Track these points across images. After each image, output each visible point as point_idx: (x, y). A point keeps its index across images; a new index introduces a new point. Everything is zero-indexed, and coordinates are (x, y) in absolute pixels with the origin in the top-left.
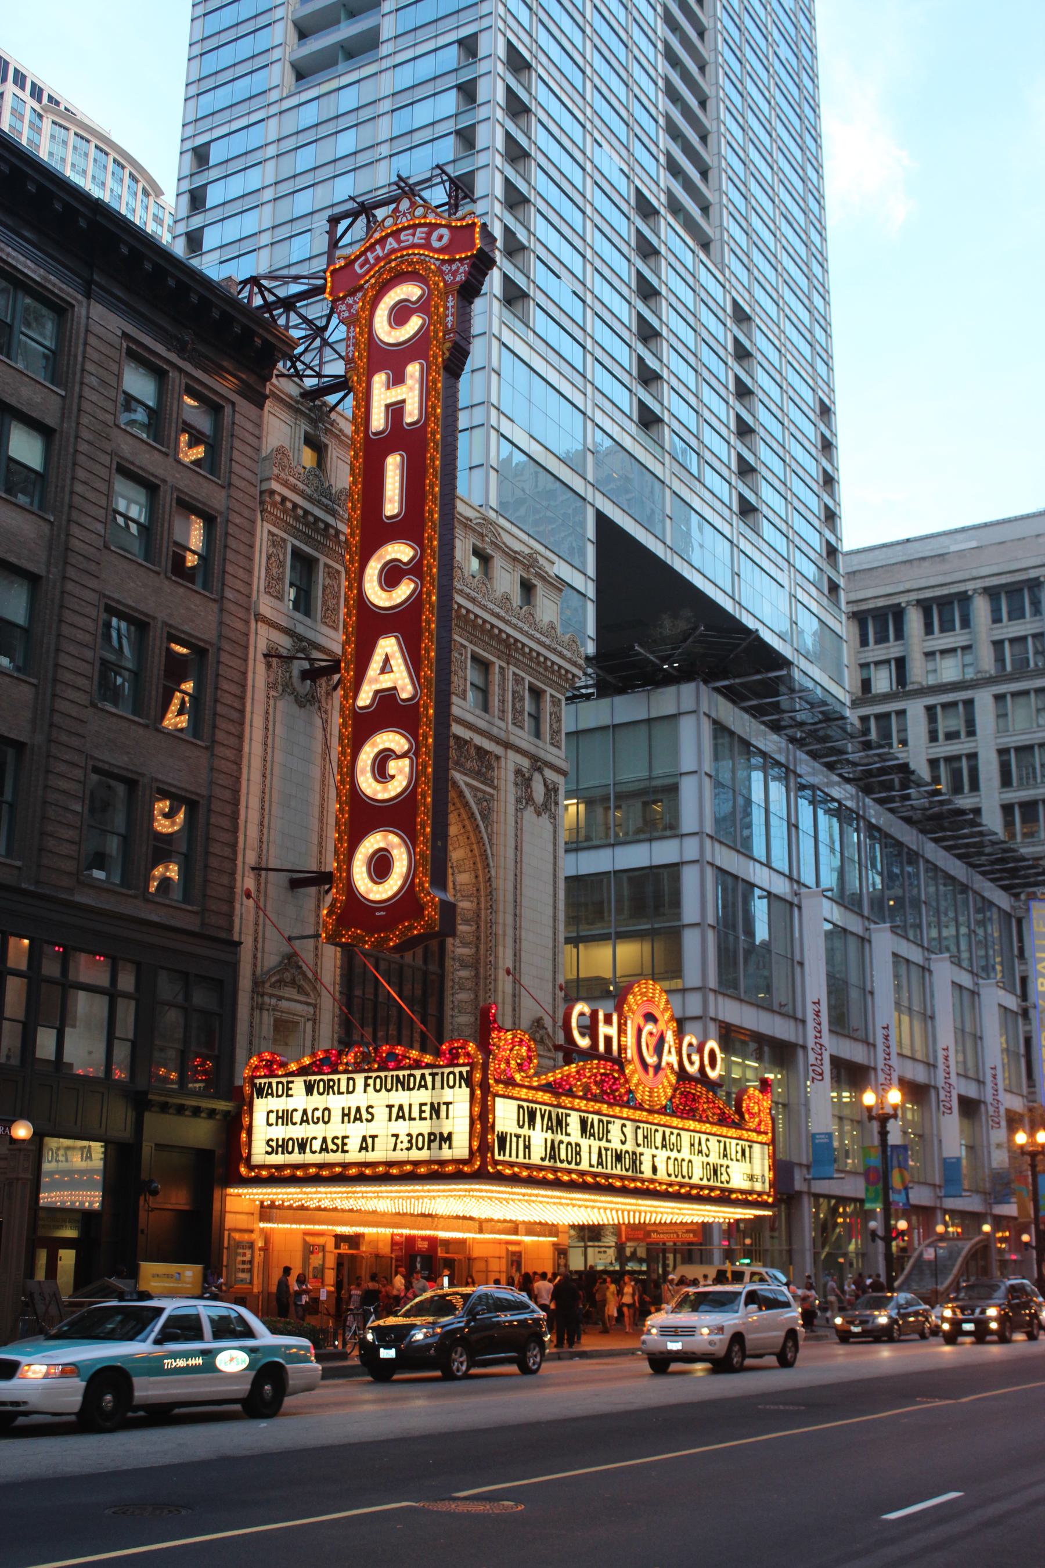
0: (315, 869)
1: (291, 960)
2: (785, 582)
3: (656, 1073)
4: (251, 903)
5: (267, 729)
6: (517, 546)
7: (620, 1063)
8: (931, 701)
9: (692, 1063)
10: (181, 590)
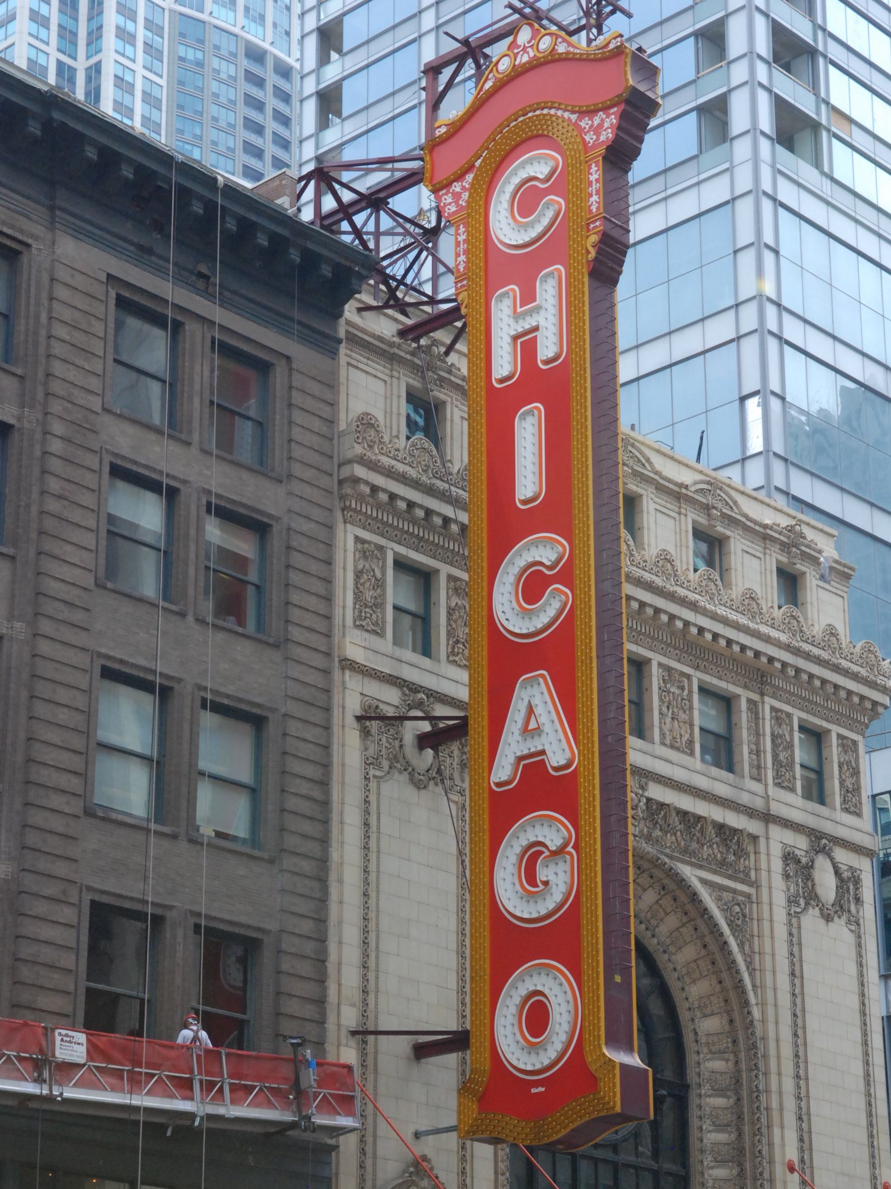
0: (455, 1029)
5: (366, 824)
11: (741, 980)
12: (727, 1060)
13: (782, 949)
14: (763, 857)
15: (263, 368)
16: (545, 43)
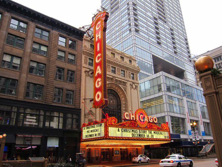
7: (135, 121)
15: (75, 42)
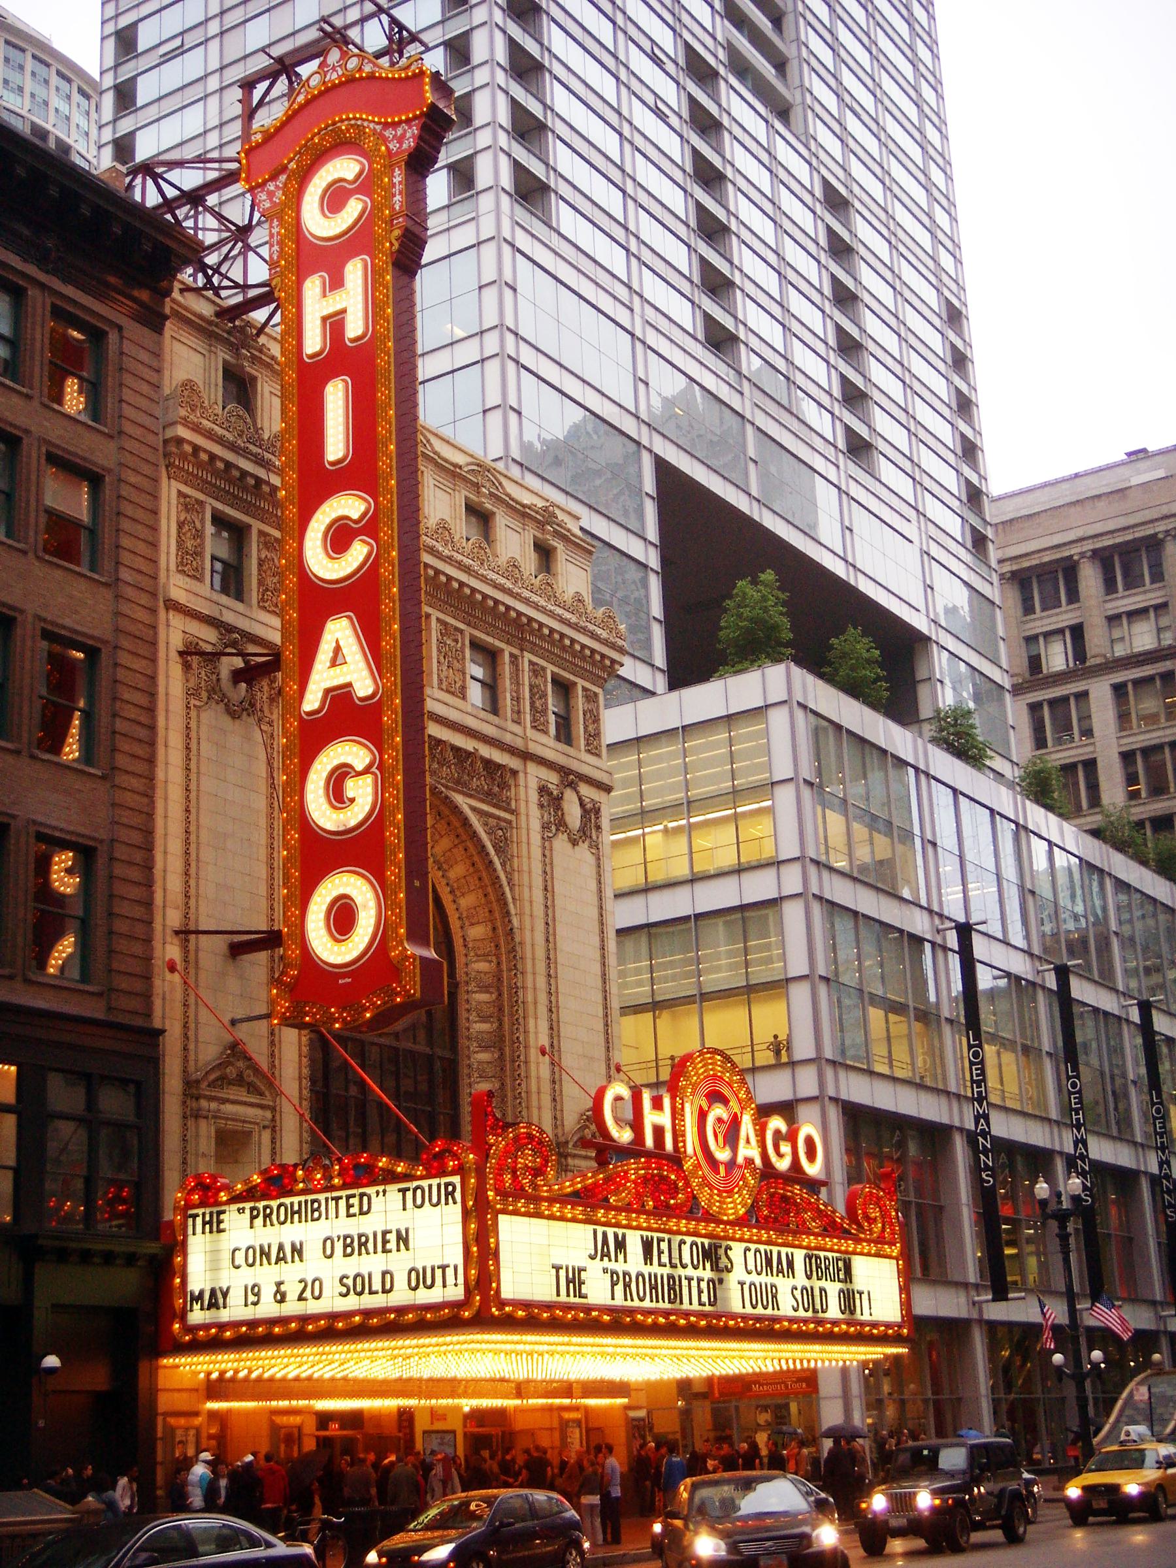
0: (265, 929)
1: (236, 1050)
2: (910, 530)
3: (728, 1172)
4: (176, 978)
5: (188, 748)
6: (527, 499)
7: (676, 1159)
8: (1120, 677)
9: (780, 1155)
10: (58, 573)
11: (503, 894)
12: (491, 962)
13: (537, 868)
14: (522, 790)
16: (353, 63)
